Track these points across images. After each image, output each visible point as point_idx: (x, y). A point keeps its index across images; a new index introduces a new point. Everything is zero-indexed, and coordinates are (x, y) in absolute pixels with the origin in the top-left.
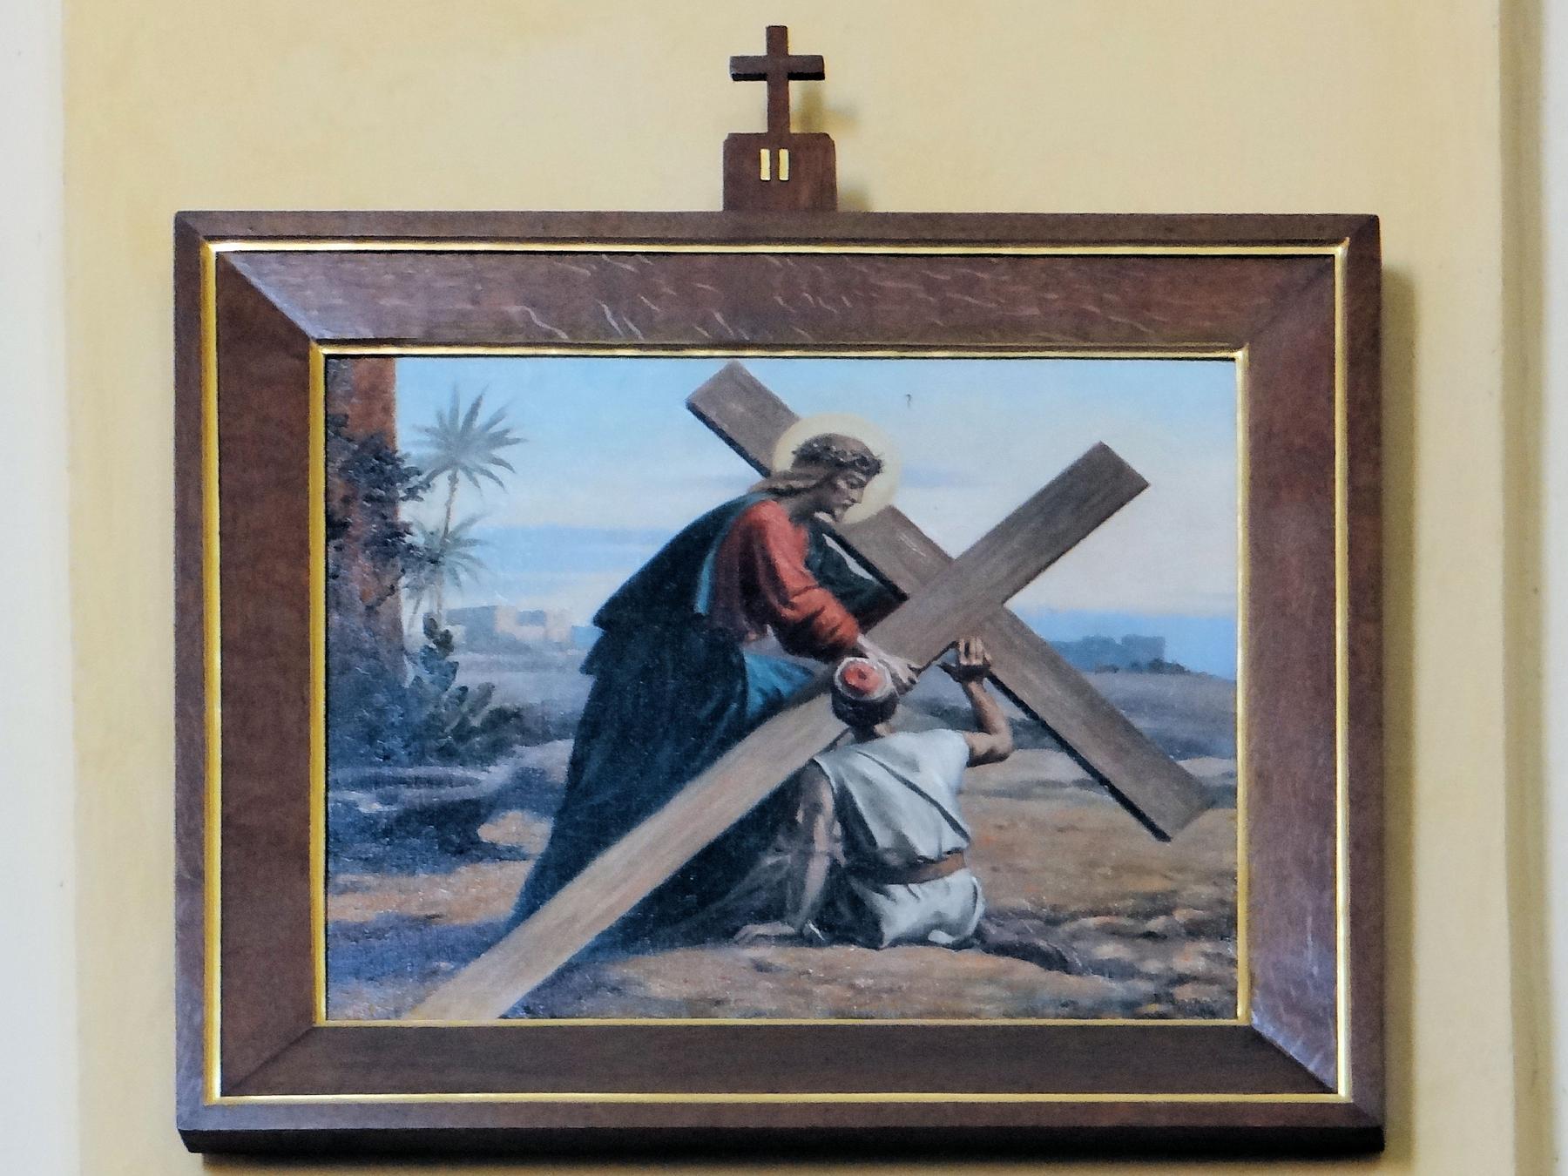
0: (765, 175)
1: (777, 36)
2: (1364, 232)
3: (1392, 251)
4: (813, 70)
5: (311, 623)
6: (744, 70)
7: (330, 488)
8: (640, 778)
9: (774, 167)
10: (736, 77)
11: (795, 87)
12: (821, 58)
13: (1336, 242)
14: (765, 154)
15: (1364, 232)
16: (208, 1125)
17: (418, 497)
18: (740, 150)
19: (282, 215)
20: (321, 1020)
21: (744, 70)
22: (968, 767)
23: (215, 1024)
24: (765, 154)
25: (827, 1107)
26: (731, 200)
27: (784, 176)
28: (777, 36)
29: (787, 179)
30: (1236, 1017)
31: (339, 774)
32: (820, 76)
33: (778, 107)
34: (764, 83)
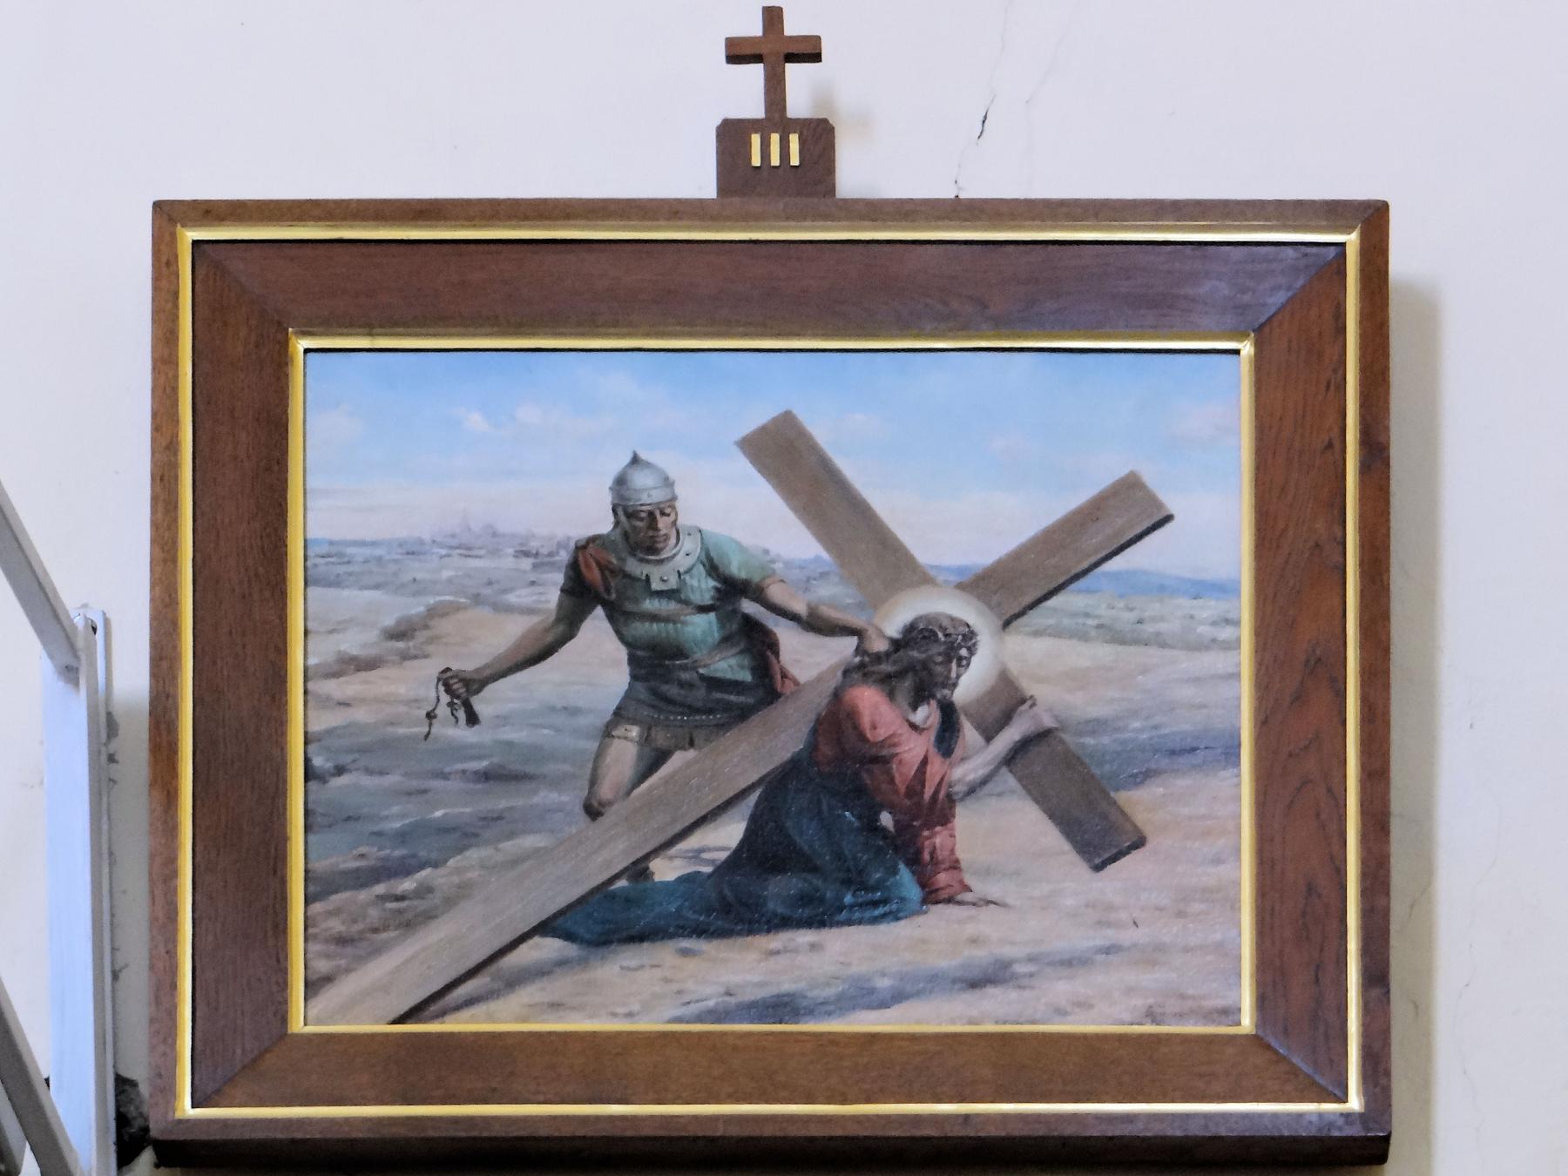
0: (756, 161)
1: (773, 17)
4: (809, 52)
5: (279, 1136)
6: (738, 53)
7: (310, 806)
11: (791, 69)
12: (727, 39)
13: (1348, 229)
14: (756, 140)
18: (732, 135)
19: (104, 855)
20: (297, 1025)
21: (738, 53)
23: (186, 988)
24: (756, 140)
26: (724, 186)
27: (795, 161)
28: (773, 17)
29: (797, 164)
30: (1239, 1024)
31: (317, 907)
33: (775, 89)
34: (761, 66)
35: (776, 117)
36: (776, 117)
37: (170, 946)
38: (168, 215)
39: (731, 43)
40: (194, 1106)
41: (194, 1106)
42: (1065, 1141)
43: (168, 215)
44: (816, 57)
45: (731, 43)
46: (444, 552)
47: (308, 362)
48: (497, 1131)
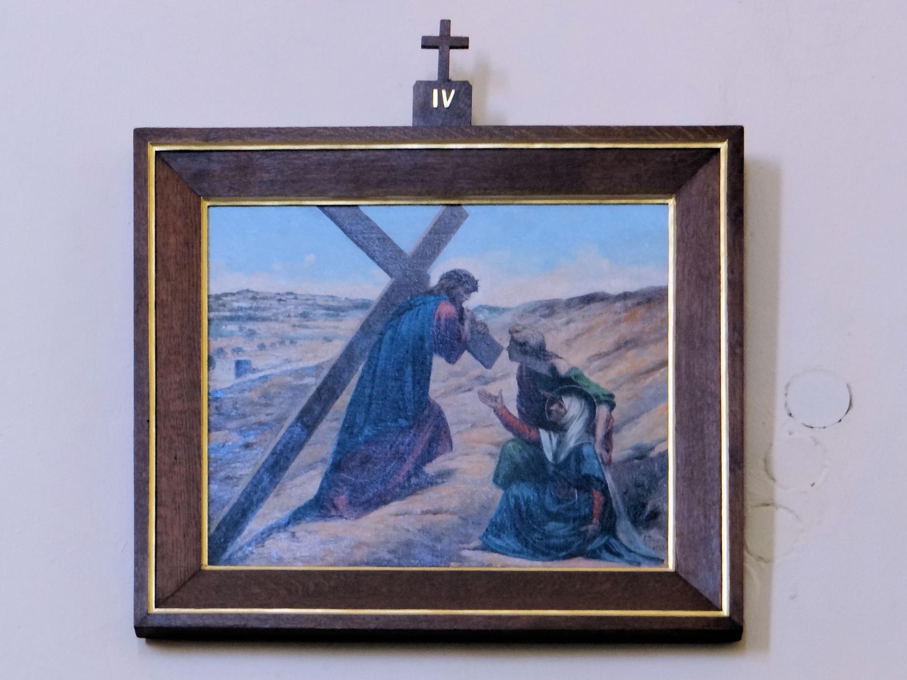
0: (435, 104)
1: (445, 25)
2: (735, 135)
3: (750, 148)
4: (463, 44)
6: (428, 43)
8: (289, 451)
9: (375, 247)
10: (424, 47)
13: (722, 141)
15: (735, 135)
16: (151, 623)
17: (254, 370)
18: (423, 90)
21: (428, 43)
22: (244, 446)
25: (377, 617)
28: (445, 25)
30: (668, 566)
32: (466, 47)
34: (436, 51)
35: (444, 81)
36: (444, 81)
37: (447, 65)
38: (142, 136)
39: (425, 39)
40: (156, 607)
41: (156, 607)
42: (678, 631)
43: (142, 136)
44: (466, 47)
45: (425, 39)
46: (189, 442)
47: (211, 215)
48: (178, 623)
